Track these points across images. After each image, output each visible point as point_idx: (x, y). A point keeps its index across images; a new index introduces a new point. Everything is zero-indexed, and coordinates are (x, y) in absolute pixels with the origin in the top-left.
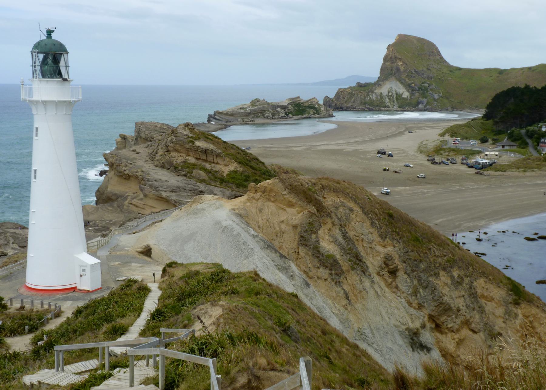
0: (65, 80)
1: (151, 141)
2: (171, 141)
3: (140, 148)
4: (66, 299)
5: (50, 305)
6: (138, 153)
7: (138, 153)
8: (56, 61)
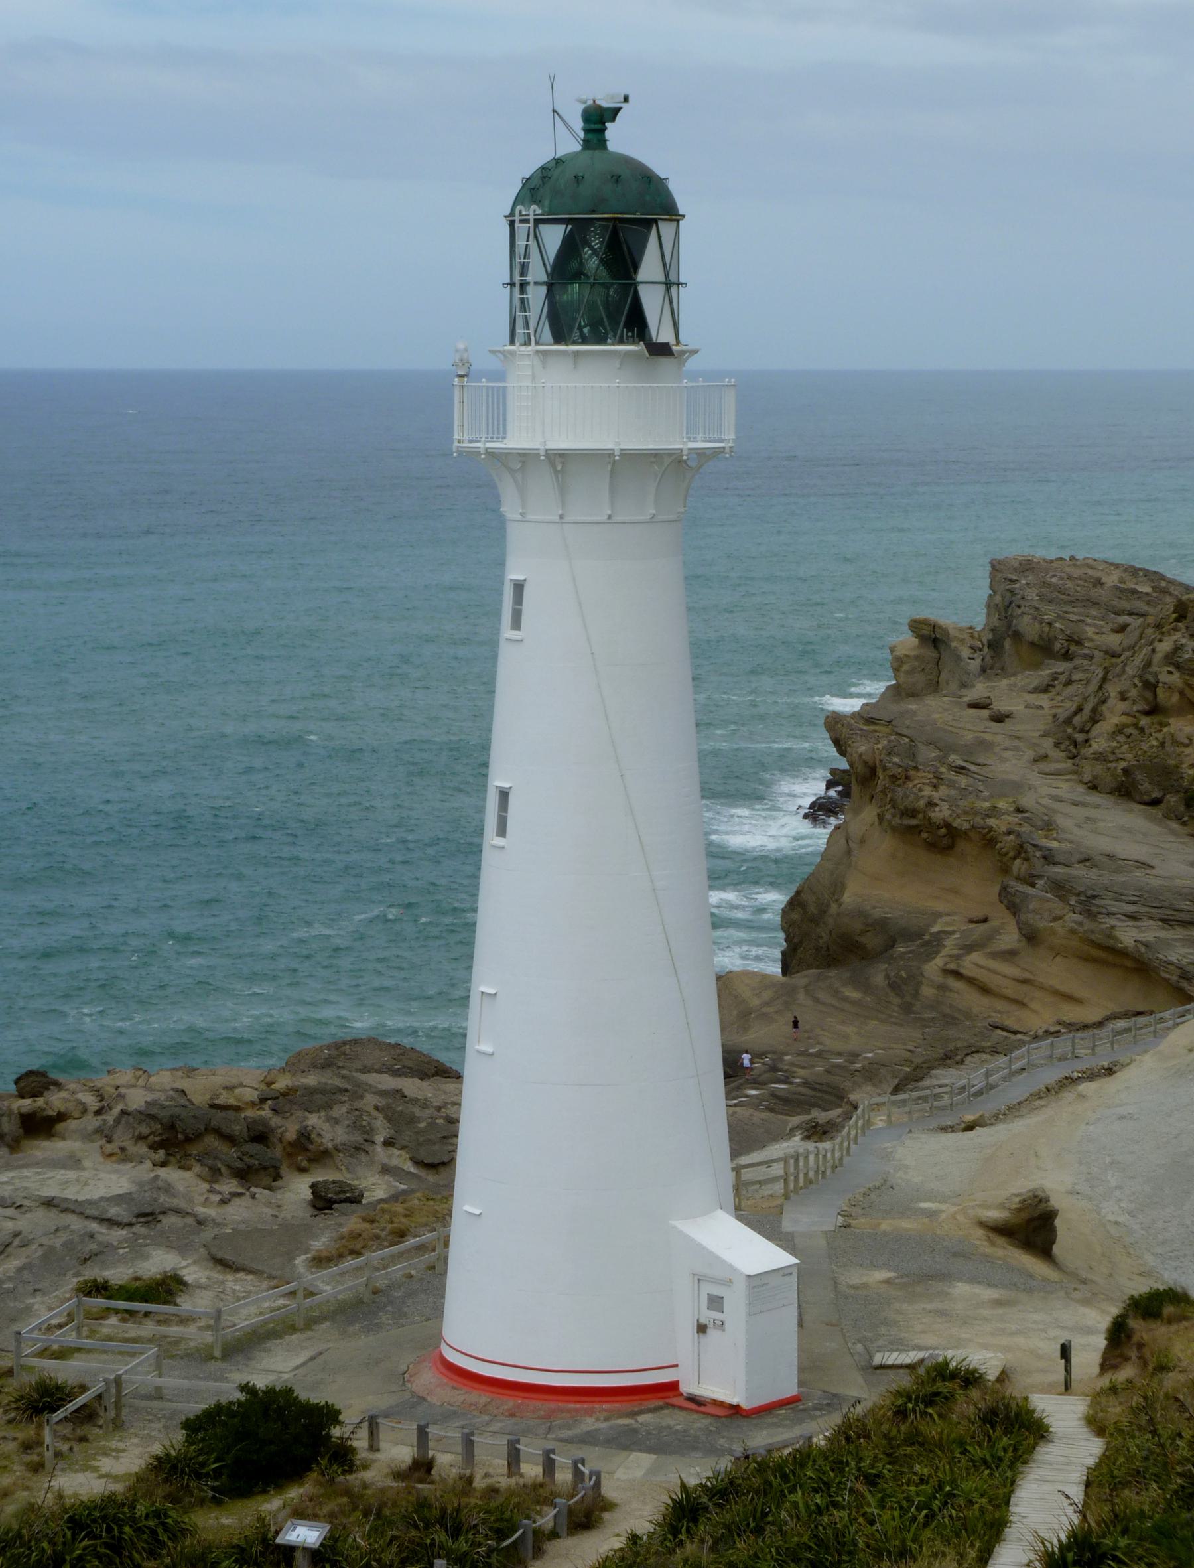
0: (661, 350)
1: (1067, 656)
2: (1171, 659)
3: (1012, 693)
4: (627, 1441)
5: (549, 1466)
6: (999, 718)
7: (999, 718)
8: (622, 260)
